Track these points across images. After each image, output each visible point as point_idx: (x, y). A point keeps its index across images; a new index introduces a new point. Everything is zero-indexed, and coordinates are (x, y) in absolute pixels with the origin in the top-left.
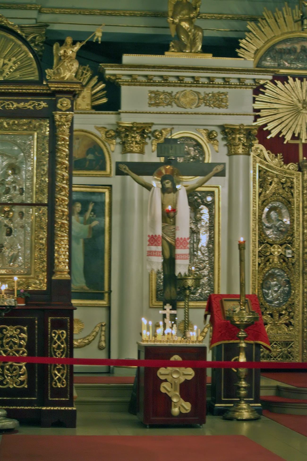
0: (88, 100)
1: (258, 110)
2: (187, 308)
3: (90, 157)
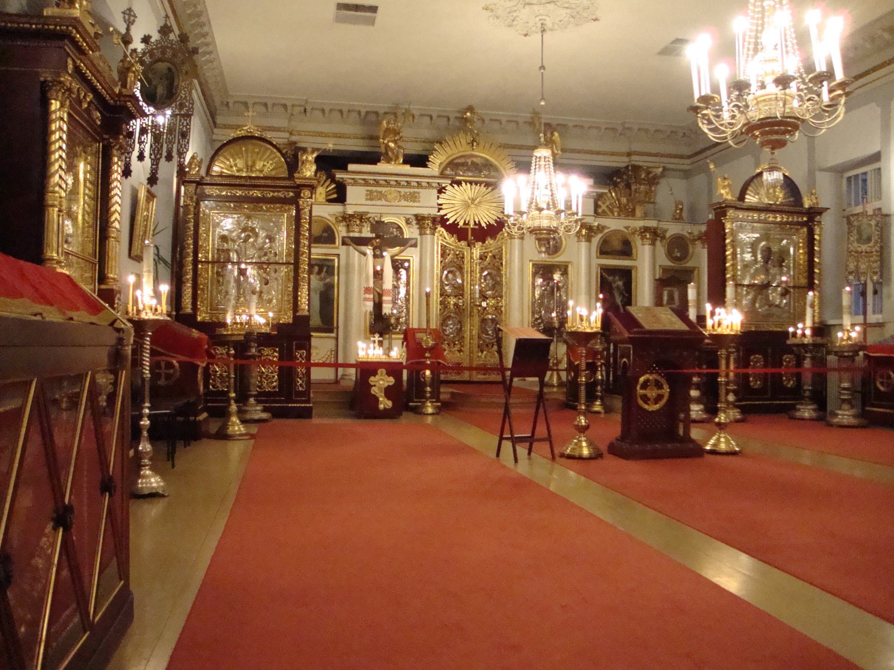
0: (324, 195)
1: (441, 205)
2: (390, 339)
3: (325, 235)
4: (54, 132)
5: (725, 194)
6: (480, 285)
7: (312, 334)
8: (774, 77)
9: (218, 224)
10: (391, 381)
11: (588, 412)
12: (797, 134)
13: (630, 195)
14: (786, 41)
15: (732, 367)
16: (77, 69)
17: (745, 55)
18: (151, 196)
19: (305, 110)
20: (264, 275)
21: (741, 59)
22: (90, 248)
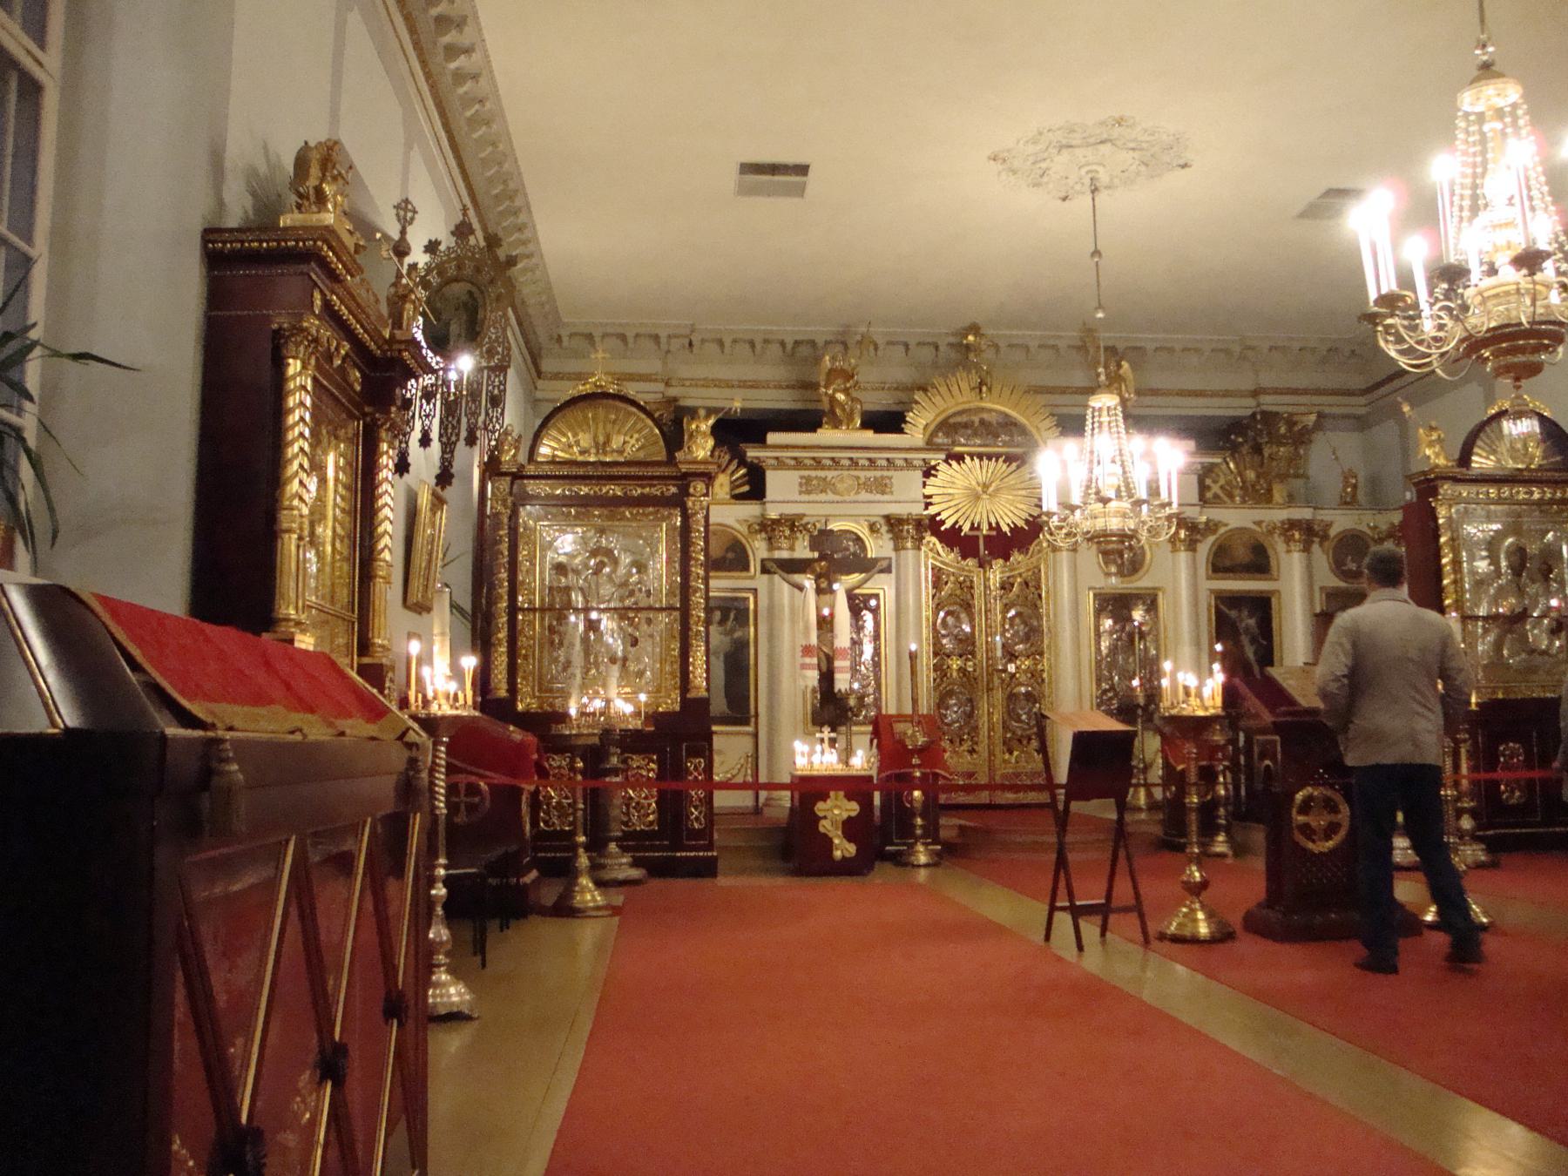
0: (727, 488)
1: (930, 497)
2: (849, 735)
3: (730, 555)
4: (292, 411)
5: (1434, 455)
6: (1003, 635)
7: (714, 728)
8: (1511, 254)
9: (551, 544)
10: (853, 808)
11: (1206, 858)
12: (1560, 349)
13: (1262, 465)
14: (1529, 189)
15: (1464, 770)
16: (327, 305)
17: (1456, 219)
18: (438, 502)
19: (691, 344)
20: (630, 630)
21: (1450, 225)
22: (343, 595)
